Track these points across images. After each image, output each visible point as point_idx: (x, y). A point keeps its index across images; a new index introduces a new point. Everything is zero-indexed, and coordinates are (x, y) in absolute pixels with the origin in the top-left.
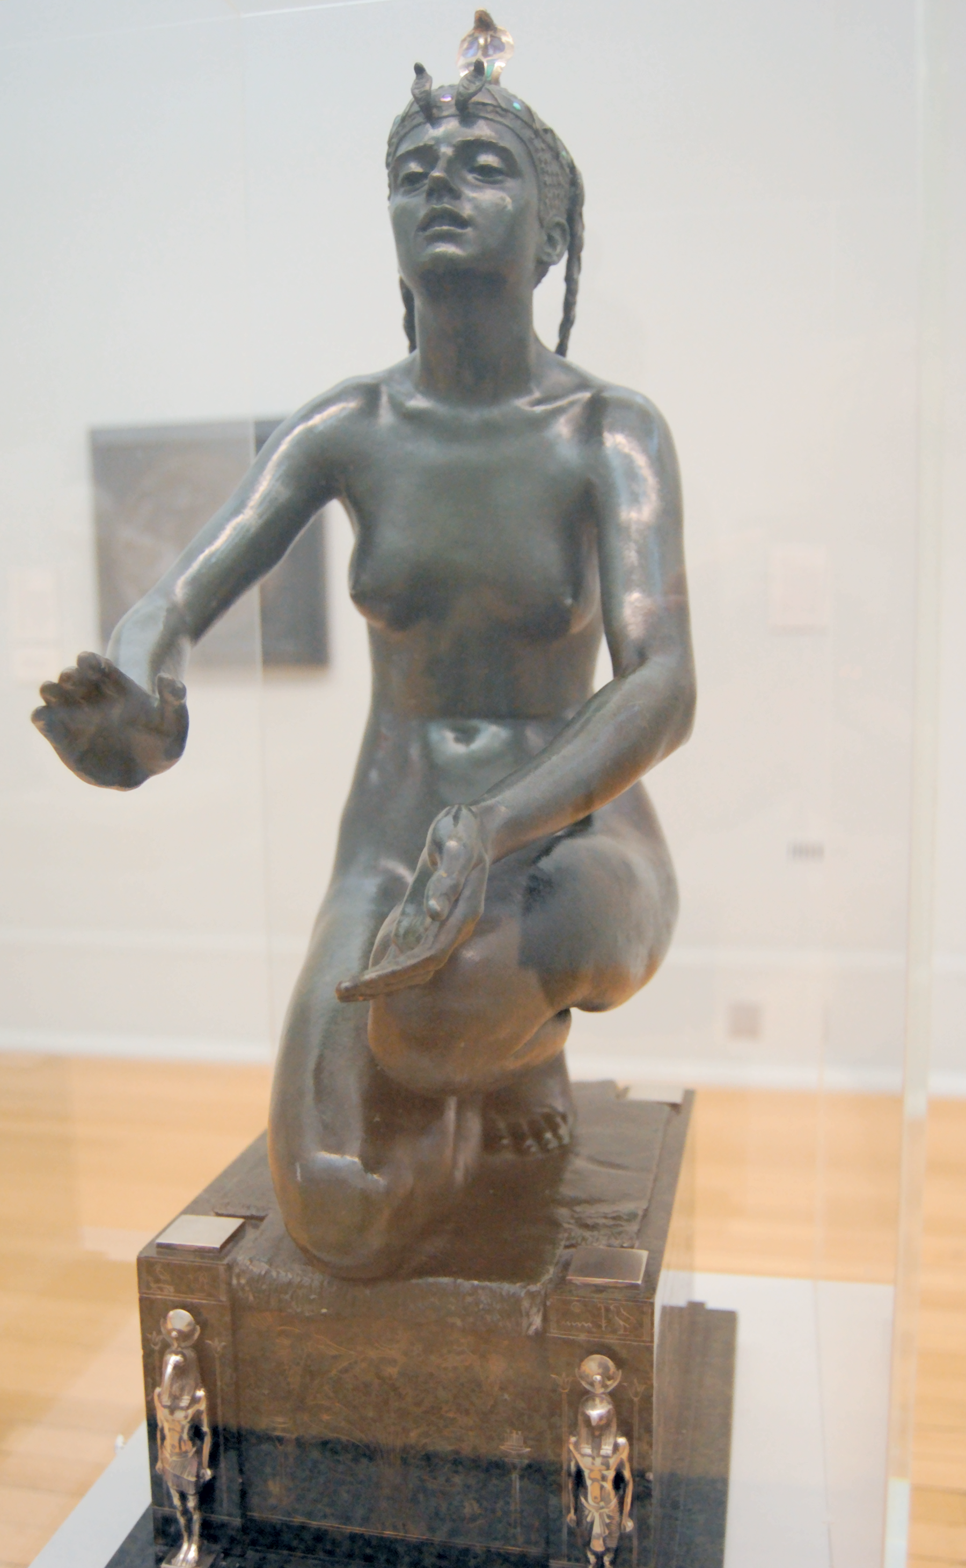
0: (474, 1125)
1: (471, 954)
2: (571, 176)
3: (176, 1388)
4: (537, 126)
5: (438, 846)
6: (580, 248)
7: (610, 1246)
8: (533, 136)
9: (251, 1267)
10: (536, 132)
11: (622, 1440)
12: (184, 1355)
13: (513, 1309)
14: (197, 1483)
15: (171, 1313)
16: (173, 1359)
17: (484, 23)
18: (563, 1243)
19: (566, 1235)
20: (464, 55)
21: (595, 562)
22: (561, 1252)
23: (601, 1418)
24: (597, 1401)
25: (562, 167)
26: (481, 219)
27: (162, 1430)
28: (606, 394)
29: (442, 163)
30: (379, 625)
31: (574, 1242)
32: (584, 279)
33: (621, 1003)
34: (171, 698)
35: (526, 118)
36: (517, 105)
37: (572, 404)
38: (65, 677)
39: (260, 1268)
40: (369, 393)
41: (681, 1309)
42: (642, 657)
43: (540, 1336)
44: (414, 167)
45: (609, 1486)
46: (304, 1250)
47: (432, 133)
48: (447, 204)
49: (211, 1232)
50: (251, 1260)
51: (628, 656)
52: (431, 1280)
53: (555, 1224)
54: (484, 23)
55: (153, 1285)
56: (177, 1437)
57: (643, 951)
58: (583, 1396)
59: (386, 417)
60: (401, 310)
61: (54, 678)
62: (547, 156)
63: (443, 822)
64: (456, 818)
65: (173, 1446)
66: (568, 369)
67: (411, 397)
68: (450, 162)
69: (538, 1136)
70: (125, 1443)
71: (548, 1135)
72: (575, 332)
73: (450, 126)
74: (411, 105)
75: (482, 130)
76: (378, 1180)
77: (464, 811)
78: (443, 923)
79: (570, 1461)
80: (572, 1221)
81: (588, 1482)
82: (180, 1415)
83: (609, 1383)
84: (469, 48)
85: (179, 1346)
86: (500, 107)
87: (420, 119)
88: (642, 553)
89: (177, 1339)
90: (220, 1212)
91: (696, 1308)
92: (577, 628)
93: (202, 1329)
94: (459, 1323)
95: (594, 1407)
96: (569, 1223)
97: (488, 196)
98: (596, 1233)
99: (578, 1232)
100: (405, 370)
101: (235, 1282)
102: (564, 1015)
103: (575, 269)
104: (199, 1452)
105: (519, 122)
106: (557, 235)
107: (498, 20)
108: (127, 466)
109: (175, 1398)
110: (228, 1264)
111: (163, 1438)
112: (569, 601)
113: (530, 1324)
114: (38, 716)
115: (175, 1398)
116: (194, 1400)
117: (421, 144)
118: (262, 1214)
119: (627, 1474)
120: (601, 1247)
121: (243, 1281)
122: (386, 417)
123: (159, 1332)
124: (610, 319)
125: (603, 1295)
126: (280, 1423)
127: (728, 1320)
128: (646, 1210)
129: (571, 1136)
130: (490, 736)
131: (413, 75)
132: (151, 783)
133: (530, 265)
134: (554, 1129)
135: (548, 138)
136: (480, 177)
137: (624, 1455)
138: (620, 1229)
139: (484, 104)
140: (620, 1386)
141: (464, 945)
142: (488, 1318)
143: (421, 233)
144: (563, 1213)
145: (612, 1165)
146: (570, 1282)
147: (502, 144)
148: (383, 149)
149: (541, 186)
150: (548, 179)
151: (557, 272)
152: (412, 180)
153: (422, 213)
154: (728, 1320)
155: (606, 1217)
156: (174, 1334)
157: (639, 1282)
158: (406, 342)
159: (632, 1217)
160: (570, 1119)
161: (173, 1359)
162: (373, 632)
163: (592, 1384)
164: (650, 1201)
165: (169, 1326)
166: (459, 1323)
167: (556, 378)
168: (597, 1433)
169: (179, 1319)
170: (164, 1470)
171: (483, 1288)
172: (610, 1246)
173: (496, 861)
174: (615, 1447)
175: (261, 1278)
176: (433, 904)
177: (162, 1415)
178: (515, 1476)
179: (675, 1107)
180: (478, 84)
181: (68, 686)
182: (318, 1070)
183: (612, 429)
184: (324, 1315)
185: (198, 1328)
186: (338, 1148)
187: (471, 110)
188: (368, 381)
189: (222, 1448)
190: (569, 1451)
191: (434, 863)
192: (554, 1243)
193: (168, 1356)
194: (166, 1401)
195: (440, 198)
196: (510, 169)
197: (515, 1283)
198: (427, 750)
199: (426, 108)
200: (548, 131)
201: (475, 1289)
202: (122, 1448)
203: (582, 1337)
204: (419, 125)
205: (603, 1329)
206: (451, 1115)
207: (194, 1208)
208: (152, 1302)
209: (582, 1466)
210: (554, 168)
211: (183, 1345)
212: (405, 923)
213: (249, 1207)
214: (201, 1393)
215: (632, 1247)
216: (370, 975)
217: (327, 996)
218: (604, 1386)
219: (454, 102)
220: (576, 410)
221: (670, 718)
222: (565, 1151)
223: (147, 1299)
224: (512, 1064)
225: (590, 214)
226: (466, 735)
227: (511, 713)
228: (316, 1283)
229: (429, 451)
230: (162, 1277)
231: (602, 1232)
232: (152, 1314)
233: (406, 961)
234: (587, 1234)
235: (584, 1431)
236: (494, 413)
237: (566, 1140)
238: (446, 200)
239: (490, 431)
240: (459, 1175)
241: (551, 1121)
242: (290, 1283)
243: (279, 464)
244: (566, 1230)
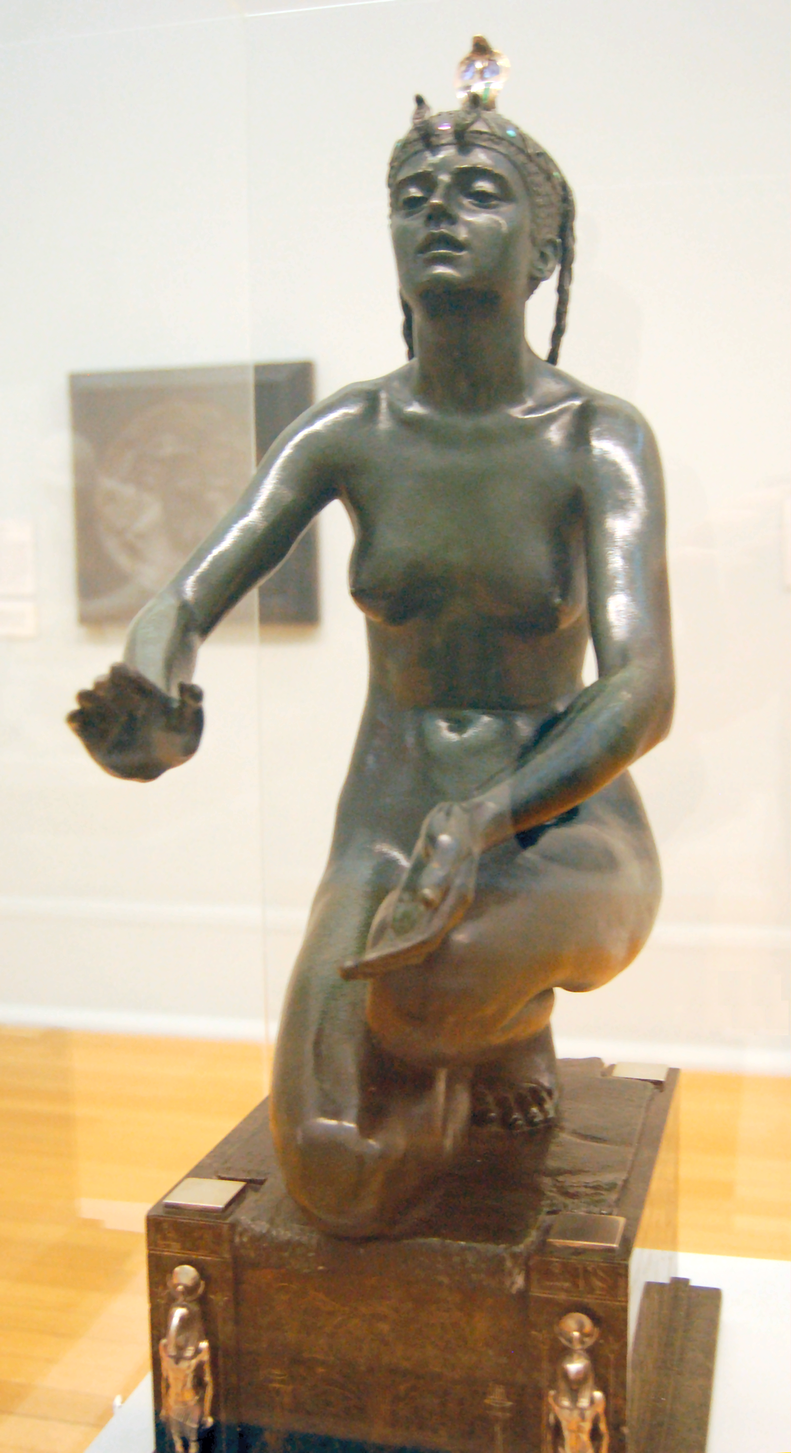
0: (463, 1104)
1: (461, 937)
2: (562, 193)
3: (182, 1339)
4: (530, 151)
5: (432, 839)
6: (571, 261)
7: (589, 1212)
8: (526, 161)
9: (253, 1226)
10: (529, 157)
11: (598, 1394)
12: (188, 1309)
13: (497, 1268)
14: (199, 1429)
15: (177, 1269)
16: (178, 1313)
17: (481, 48)
18: (546, 1209)
19: (549, 1202)
20: (462, 77)
21: (582, 562)
22: (544, 1218)
23: (578, 1373)
24: (575, 1356)
25: (554, 187)
26: (477, 232)
27: (167, 1380)
28: (596, 403)
29: (440, 191)
30: (377, 620)
31: (555, 1208)
32: (575, 290)
33: (603, 984)
34: (190, 702)
35: (520, 144)
36: (511, 133)
37: (562, 412)
38: (99, 685)
39: (261, 1227)
40: (369, 397)
41: (662, 1285)
42: (625, 659)
43: (523, 1295)
44: (414, 192)
45: (585, 1437)
46: (304, 1210)
47: (432, 159)
48: (444, 229)
49: (214, 1194)
50: (253, 1220)
51: (612, 657)
52: (421, 1240)
53: (538, 1192)
54: (481, 48)
55: (161, 1242)
56: (180, 1385)
57: (625, 935)
58: (564, 1352)
59: (384, 423)
60: (399, 317)
61: (89, 686)
62: (540, 178)
63: (435, 817)
64: (448, 814)
65: (177, 1394)
66: (560, 377)
67: (410, 404)
68: (449, 187)
69: (525, 1111)
70: (123, 1402)
71: (535, 1110)
72: (566, 341)
73: (447, 153)
74: (411, 132)
75: (480, 158)
76: (374, 1144)
77: (456, 809)
78: (436, 909)
79: (548, 1414)
80: (554, 1189)
81: (566, 1433)
82: (184, 1365)
83: (587, 1339)
84: (466, 71)
85: (185, 1300)
86: (495, 135)
87: (419, 146)
88: (628, 557)
89: (183, 1293)
90: (223, 1176)
91: (679, 1285)
92: (565, 624)
93: (207, 1285)
94: (445, 1280)
95: (571, 1362)
96: (551, 1191)
97: (481, 218)
98: (576, 1201)
99: (561, 1199)
100: (403, 376)
101: (237, 1240)
102: (547, 994)
103: (566, 279)
104: (201, 1401)
105: (513, 149)
106: (549, 251)
107: (495, 44)
108: (112, 415)
109: (181, 1349)
110: (230, 1224)
111: (168, 1387)
112: (558, 600)
113: (513, 1283)
114: (74, 718)
115: (181, 1349)
116: (198, 1351)
117: (420, 171)
118: (263, 1178)
119: (603, 1427)
120: (582, 1213)
121: (245, 1239)
122: (384, 423)
123: (165, 1286)
124: (602, 329)
125: (579, 1257)
126: (277, 1375)
127: (713, 1296)
128: (626, 1181)
129: (557, 1111)
130: (483, 725)
131: (413, 106)
132: (169, 776)
133: (522, 281)
134: (540, 1103)
135: (541, 161)
136: (476, 202)
137: (600, 1409)
138: (602, 1197)
139: (481, 133)
140: (596, 1344)
141: (454, 929)
142: (474, 1276)
143: (420, 255)
144: (547, 1182)
145: (594, 1139)
146: (551, 1245)
147: (497, 171)
148: (383, 170)
149: (534, 206)
150: (540, 200)
151: (547, 289)
152: (412, 204)
153: (421, 236)
154: (713, 1296)
155: (586, 1187)
156: (180, 1288)
157: (614, 1245)
158: (403, 348)
159: (611, 1187)
160: (556, 1095)
161: (178, 1313)
162: (370, 625)
163: (570, 1340)
164: (630, 1173)
165: (175, 1281)
166: (445, 1280)
167: (549, 387)
168: (574, 1388)
169: (186, 1274)
170: (168, 1418)
171: (469, 1249)
172: (589, 1212)
173: (484, 852)
174: (593, 1398)
175: (263, 1237)
176: (428, 892)
177: (167, 1364)
178: (497, 1428)
179: (658, 1084)
180: (474, 115)
181: (101, 693)
182: (317, 1043)
183: (600, 436)
184: (321, 1271)
185: (202, 1283)
186: (336, 1114)
187: (468, 138)
188: (366, 387)
189: (222, 1399)
190: (548, 1404)
191: (428, 855)
192: (537, 1210)
193: (174, 1309)
194: (172, 1351)
195: (438, 225)
196: (504, 194)
197: (498, 1244)
198: (421, 737)
199: (424, 136)
200: (542, 155)
201: (464, 1249)
202: (120, 1407)
203: (562, 1297)
204: (416, 153)
205: (581, 1289)
206: (441, 1086)
207: (199, 1172)
208: (159, 1258)
209: (561, 1418)
210: (546, 188)
211: (189, 1298)
212: (402, 909)
213: (249, 1172)
214: (204, 1345)
215: (610, 1214)
216: (371, 955)
217: (328, 973)
218: (582, 1342)
219: (452, 130)
220: (566, 419)
221: (651, 718)
222: (550, 1127)
223: (156, 1256)
224: (498, 1039)
225: (580, 227)
226: (459, 726)
227: (503, 706)
228: (314, 1242)
229: (425, 456)
230: (169, 1235)
231: (583, 1200)
232: (159, 1270)
233: (403, 944)
234: (568, 1201)
235: (562, 1385)
236: (488, 421)
237: (552, 1114)
238: (443, 225)
239: (483, 438)
240: (448, 1143)
241: (537, 1096)
242: (289, 1242)
243: (284, 468)
244: (549, 1198)
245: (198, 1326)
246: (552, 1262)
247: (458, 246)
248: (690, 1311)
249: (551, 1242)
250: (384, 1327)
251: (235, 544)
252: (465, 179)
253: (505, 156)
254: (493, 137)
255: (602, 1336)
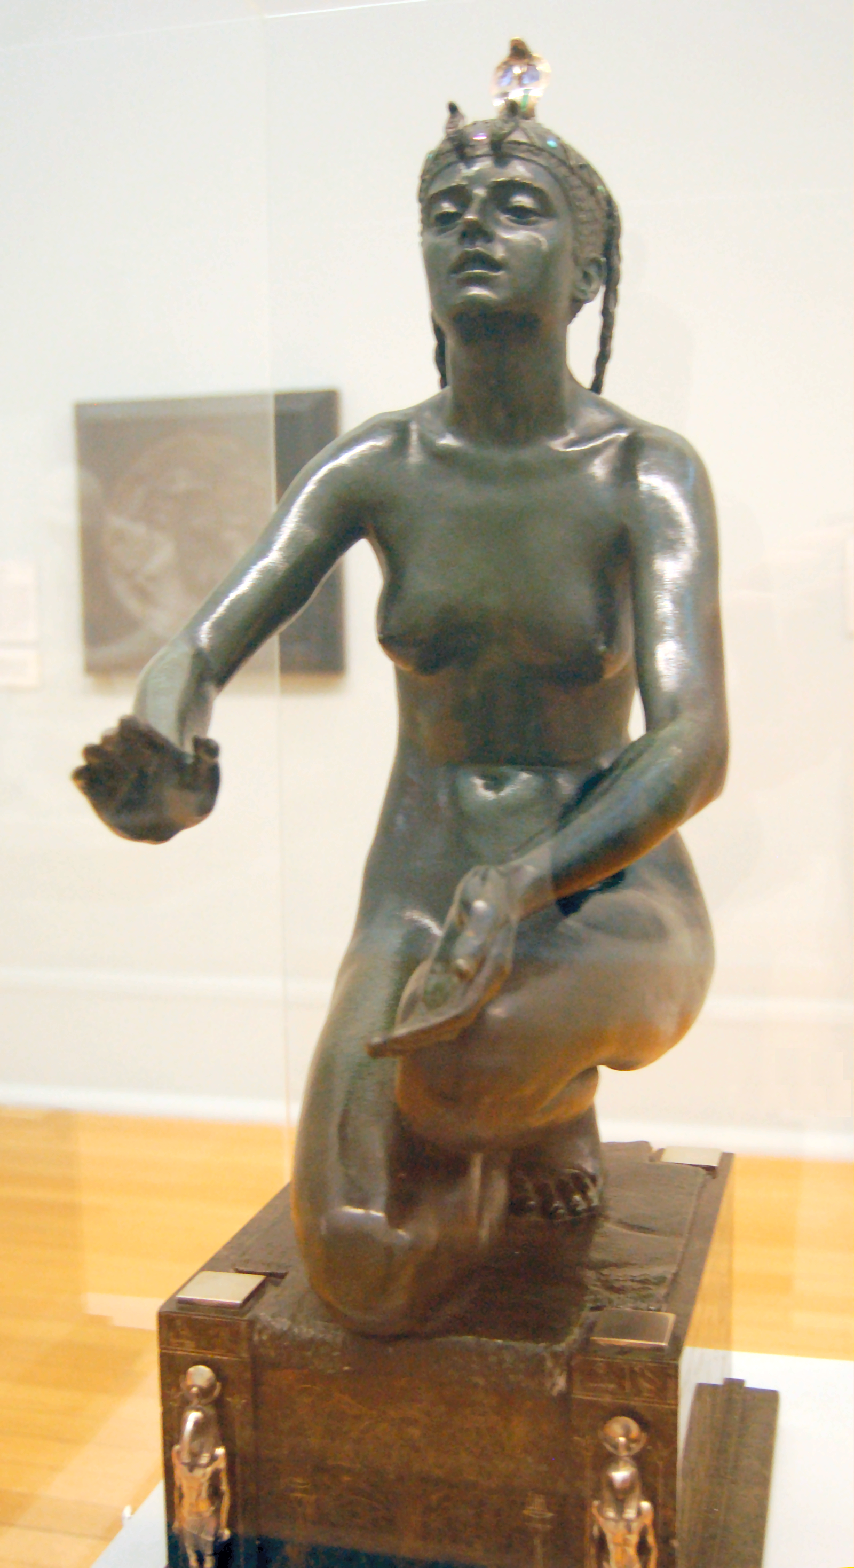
0: (500, 1191)
1: (498, 1011)
2: (607, 208)
3: (196, 1445)
4: (572, 163)
5: (466, 906)
6: (616, 282)
7: (636, 1308)
8: (568, 174)
9: (273, 1323)
10: (571, 169)
11: (646, 1505)
12: (203, 1412)
13: (536, 1369)
14: (215, 1542)
15: (191, 1370)
16: (193, 1417)
17: (519, 52)
18: (589, 1305)
19: (592, 1297)
20: (499, 83)
21: (628, 606)
22: (587, 1315)
23: (624, 1481)
24: (621, 1463)
25: (598, 202)
26: (515, 250)
27: (180, 1489)
28: (644, 435)
29: (475, 206)
30: (408, 669)
31: (599, 1304)
32: (621, 313)
33: (651, 1061)
34: (205, 757)
35: (561, 155)
36: (552, 143)
37: (607, 445)
38: (107, 740)
39: (282, 1324)
40: (399, 428)
42: (674, 711)
43: (565, 1397)
44: (447, 207)
45: (632, 1551)
46: (328, 1306)
47: (467, 172)
48: (480, 247)
49: (231, 1289)
50: (273, 1316)
51: (661, 709)
52: (455, 1338)
53: (581, 1286)
54: (519, 52)
55: (174, 1341)
56: (194, 1495)
57: (674, 1009)
58: (609, 1459)
59: (415, 456)
60: (431, 343)
61: (96, 740)
62: (583, 193)
63: (470, 881)
64: (484, 878)
65: (191, 1505)
66: (605, 407)
67: (442, 436)
68: (485, 202)
69: (567, 1199)
70: (132, 1513)
71: (577, 1197)
72: (611, 368)
73: (483, 165)
74: (444, 142)
75: (518, 170)
76: (403, 1234)
77: (493, 873)
78: (471, 981)
79: (592, 1526)
80: (599, 1284)
81: (611, 1547)
82: (198, 1473)
83: (633, 1445)
84: (503, 77)
85: (199, 1403)
86: (535, 146)
87: (453, 157)
88: (678, 602)
89: (198, 1395)
90: (241, 1269)
91: (733, 1386)
92: (610, 673)
93: (223, 1387)
94: (481, 1381)
95: (617, 1469)
96: (595, 1285)
97: (520, 236)
98: (622, 1296)
99: (605, 1294)
100: (435, 406)
101: (256, 1338)
102: (591, 1073)
103: (611, 301)
104: (217, 1511)
105: (554, 161)
106: (592, 271)
107: (534, 48)
108: (120, 448)
109: (195, 1455)
110: (248, 1321)
111: (181, 1497)
112: (602, 648)
113: (554, 1385)
114: (80, 774)
115: (195, 1455)
116: (213, 1458)
117: (454, 184)
118: (284, 1271)
119: (651, 1539)
120: (628, 1309)
121: (265, 1337)
122: (415, 456)
123: (178, 1388)
124: (650, 355)
125: (626, 1357)
126: (299, 1484)
127: (770, 1399)
128: (676, 1275)
129: (601, 1199)
130: (522, 783)
132: (182, 838)
133: (564, 304)
134: (583, 1190)
135: (584, 173)
136: (514, 218)
137: (648, 1520)
138: (650, 1292)
139: (519, 143)
140: (644, 1450)
141: (491, 1002)
142: (512, 1377)
143: (453, 275)
144: (590, 1275)
145: (641, 1229)
146: (595, 1343)
147: (537, 184)
148: (414, 184)
149: (576, 223)
150: (583, 216)
151: (591, 312)
152: (445, 220)
153: (455, 254)
154: (770, 1399)
155: (633, 1281)
156: (195, 1390)
157: (663, 1344)
158: (435, 376)
159: (660, 1281)
160: (600, 1182)
161: (193, 1417)
162: (400, 675)
163: (616, 1446)
164: (680, 1265)
165: (189, 1383)
166: (481, 1381)
167: (592, 417)
168: (620, 1498)
169: (200, 1375)
170: (181, 1530)
171: (507, 1347)
172: (636, 1308)
173: (522, 920)
174: (640, 1508)
175: (283, 1335)
176: (462, 963)
177: (180, 1472)
178: (537, 1541)
179: (710, 1169)
180: (512, 124)
181: (109, 748)
182: (343, 1126)
183: (648, 471)
184: (346, 1372)
185: (218, 1384)
186: (362, 1203)
187: (505, 149)
188: (395, 418)
189: (240, 1510)
190: (592, 1515)
191: (462, 923)
192: (580, 1306)
193: (188, 1413)
194: (186, 1458)
195: (472, 243)
196: (545, 210)
197: (538, 1343)
198: (455, 795)
199: (458, 147)
200: (585, 167)
201: (500, 1348)
202: (130, 1518)
203: (607, 1399)
204: (449, 165)
205: (627, 1391)
206: (476, 1172)
207: (214, 1264)
208: (172, 1357)
209: (606, 1530)
210: (590, 203)
211: (204, 1401)
212: (434, 980)
213: (269, 1265)
214: (220, 1451)
215: (659, 1310)
216: (401, 1031)
217: (354, 1050)
218: (628, 1448)
219: (488, 141)
220: (611, 452)
221: (703, 775)
222: (594, 1216)
223: (168, 1355)
224: (537, 1121)
225: (626, 245)
226: (495, 783)
227: (543, 762)
228: (339, 1340)
229: (459, 492)
230: (183, 1333)
231: (629, 1295)
232: (172, 1370)
233: (435, 1019)
234: (614, 1296)
235: (607, 1494)
236: (527, 454)
237: (596, 1202)
238: (478, 243)
239: (521, 473)
240: (484, 1234)
241: (580, 1183)
242: (312, 1341)
243: (307, 505)
244: (592, 1293)
245: (214, 1431)
246: (596, 1362)
247: (495, 265)
248: (745, 1415)
249: (594, 1341)
250: (415, 1432)
251: (254, 587)
252: (502, 193)
253: (545, 168)
254: (532, 148)
255: (650, 1442)
